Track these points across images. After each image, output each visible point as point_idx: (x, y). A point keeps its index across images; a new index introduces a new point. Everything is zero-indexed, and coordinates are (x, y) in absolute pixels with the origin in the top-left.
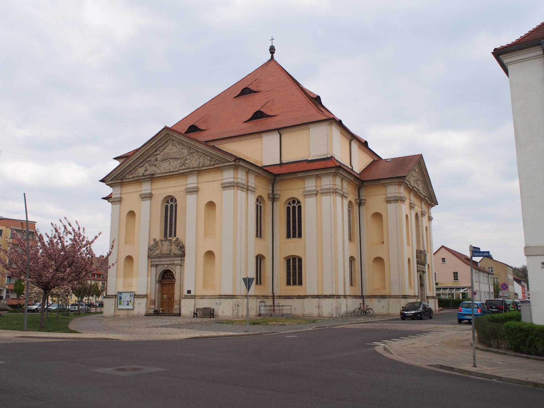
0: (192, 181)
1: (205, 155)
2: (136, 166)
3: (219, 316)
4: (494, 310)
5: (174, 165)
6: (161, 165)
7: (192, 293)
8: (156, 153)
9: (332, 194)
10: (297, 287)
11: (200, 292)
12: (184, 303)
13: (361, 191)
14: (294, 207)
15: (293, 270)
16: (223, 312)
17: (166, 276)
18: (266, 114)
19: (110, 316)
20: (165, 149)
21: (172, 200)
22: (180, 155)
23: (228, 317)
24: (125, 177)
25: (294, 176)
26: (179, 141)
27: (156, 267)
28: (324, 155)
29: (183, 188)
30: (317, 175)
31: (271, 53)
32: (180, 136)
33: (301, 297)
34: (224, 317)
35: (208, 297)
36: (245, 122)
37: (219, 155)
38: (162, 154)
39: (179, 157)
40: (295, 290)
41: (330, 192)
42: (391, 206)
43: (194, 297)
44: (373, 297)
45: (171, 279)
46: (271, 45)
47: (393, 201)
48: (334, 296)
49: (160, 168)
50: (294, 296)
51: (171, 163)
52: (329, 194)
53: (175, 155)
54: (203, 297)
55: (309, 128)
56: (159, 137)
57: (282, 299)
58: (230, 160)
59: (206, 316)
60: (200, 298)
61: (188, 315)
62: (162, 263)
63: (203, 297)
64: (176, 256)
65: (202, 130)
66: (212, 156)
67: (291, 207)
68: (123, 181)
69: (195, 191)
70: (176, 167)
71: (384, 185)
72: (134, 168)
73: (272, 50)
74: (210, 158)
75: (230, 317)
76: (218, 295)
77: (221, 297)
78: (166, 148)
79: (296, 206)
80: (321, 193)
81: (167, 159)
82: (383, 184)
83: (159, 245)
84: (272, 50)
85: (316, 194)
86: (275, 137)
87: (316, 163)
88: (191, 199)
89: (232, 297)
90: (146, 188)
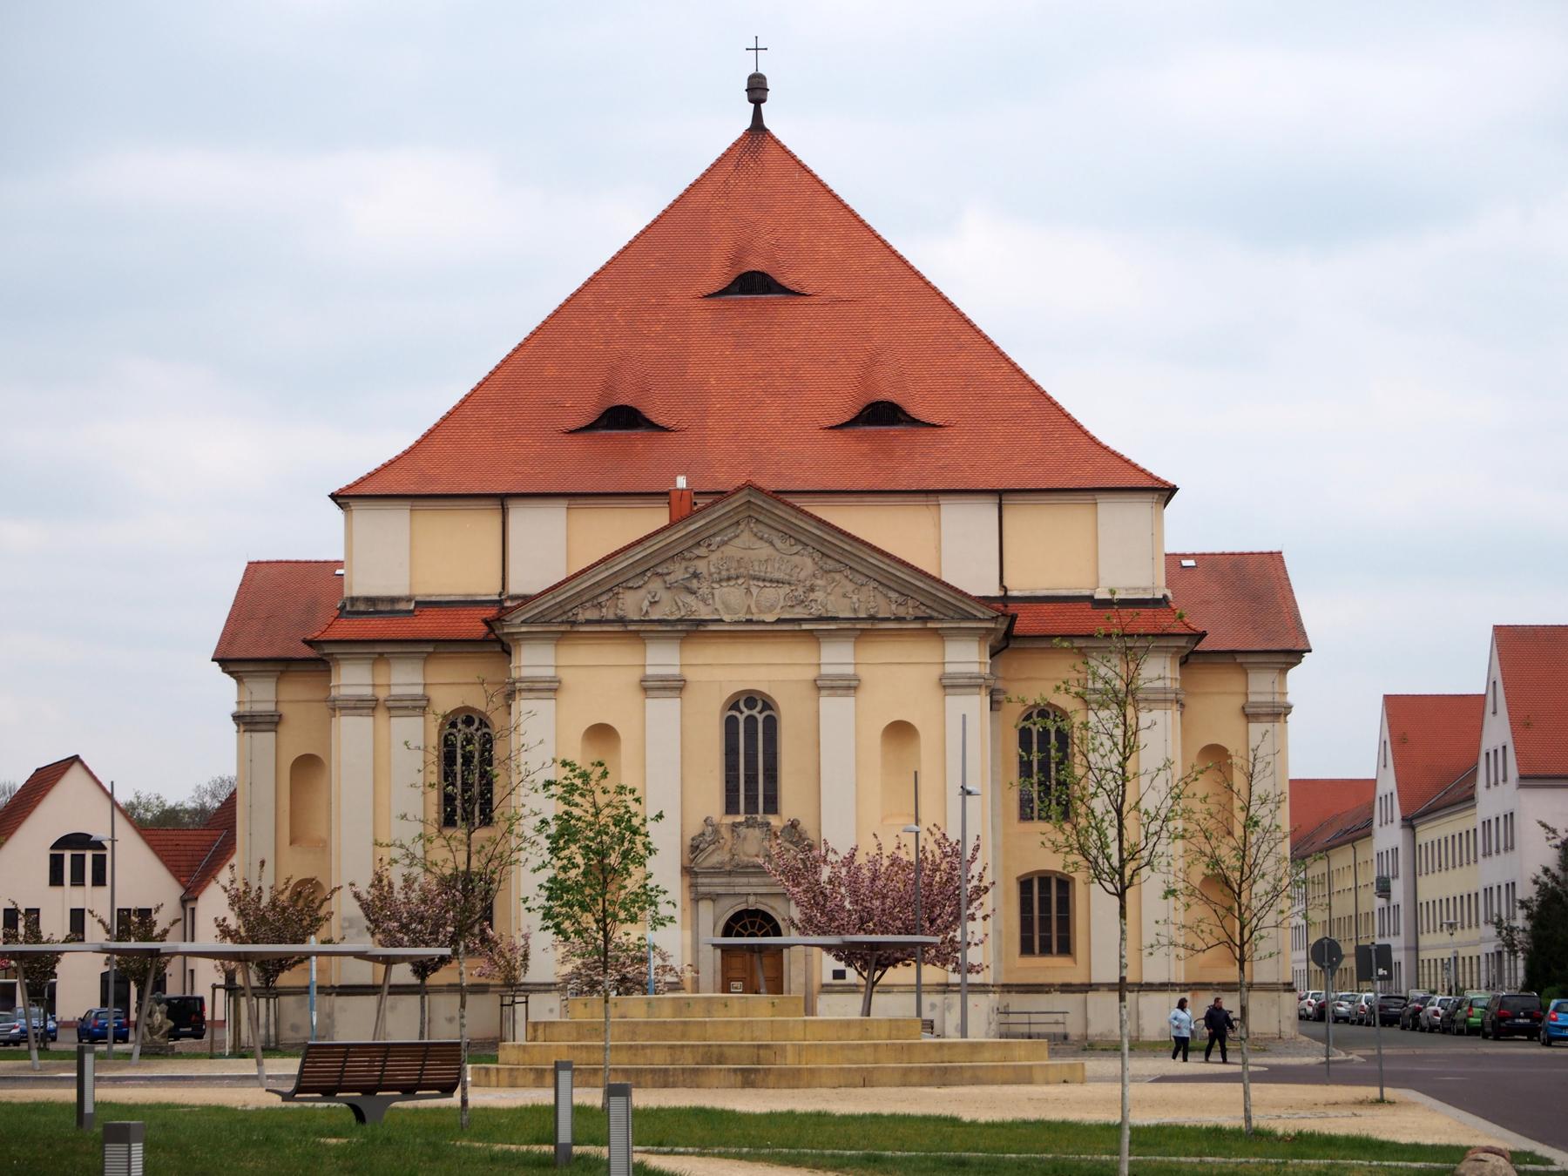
0: (837, 657)
1: (880, 583)
4: (1521, 1021)
5: (771, 603)
6: (716, 592)
8: (697, 552)
9: (1169, 705)
14: (751, 720)
15: (1041, 911)
17: (747, 921)
18: (909, 416)
20: (725, 543)
21: (469, 721)
22: (788, 571)
24: (570, 614)
25: (1044, 644)
26: (785, 530)
27: (714, 901)
28: (1145, 589)
29: (811, 674)
30: (381, 654)
31: (751, 101)
32: (801, 520)
33: (1073, 989)
35: (902, 989)
37: (941, 595)
38: (714, 557)
39: (787, 577)
40: (1053, 967)
41: (1165, 701)
42: (1256, 729)
44: (1198, 987)
46: (754, 71)
47: (1268, 715)
48: (1173, 984)
49: (711, 602)
50: (1052, 985)
51: (755, 591)
52: (1162, 705)
53: (769, 569)
56: (718, 510)
57: (1013, 994)
58: (980, 615)
62: (738, 890)
65: (662, 427)
66: (906, 592)
67: (741, 718)
68: (575, 629)
69: (848, 686)
70: (771, 609)
71: (1244, 669)
72: (611, 590)
73: (757, 89)
76: (934, 982)
78: (731, 543)
81: (737, 578)
82: (1241, 664)
84: (757, 89)
85: (374, 709)
86: (982, 514)
88: (834, 708)
89: (546, 988)
90: (663, 659)
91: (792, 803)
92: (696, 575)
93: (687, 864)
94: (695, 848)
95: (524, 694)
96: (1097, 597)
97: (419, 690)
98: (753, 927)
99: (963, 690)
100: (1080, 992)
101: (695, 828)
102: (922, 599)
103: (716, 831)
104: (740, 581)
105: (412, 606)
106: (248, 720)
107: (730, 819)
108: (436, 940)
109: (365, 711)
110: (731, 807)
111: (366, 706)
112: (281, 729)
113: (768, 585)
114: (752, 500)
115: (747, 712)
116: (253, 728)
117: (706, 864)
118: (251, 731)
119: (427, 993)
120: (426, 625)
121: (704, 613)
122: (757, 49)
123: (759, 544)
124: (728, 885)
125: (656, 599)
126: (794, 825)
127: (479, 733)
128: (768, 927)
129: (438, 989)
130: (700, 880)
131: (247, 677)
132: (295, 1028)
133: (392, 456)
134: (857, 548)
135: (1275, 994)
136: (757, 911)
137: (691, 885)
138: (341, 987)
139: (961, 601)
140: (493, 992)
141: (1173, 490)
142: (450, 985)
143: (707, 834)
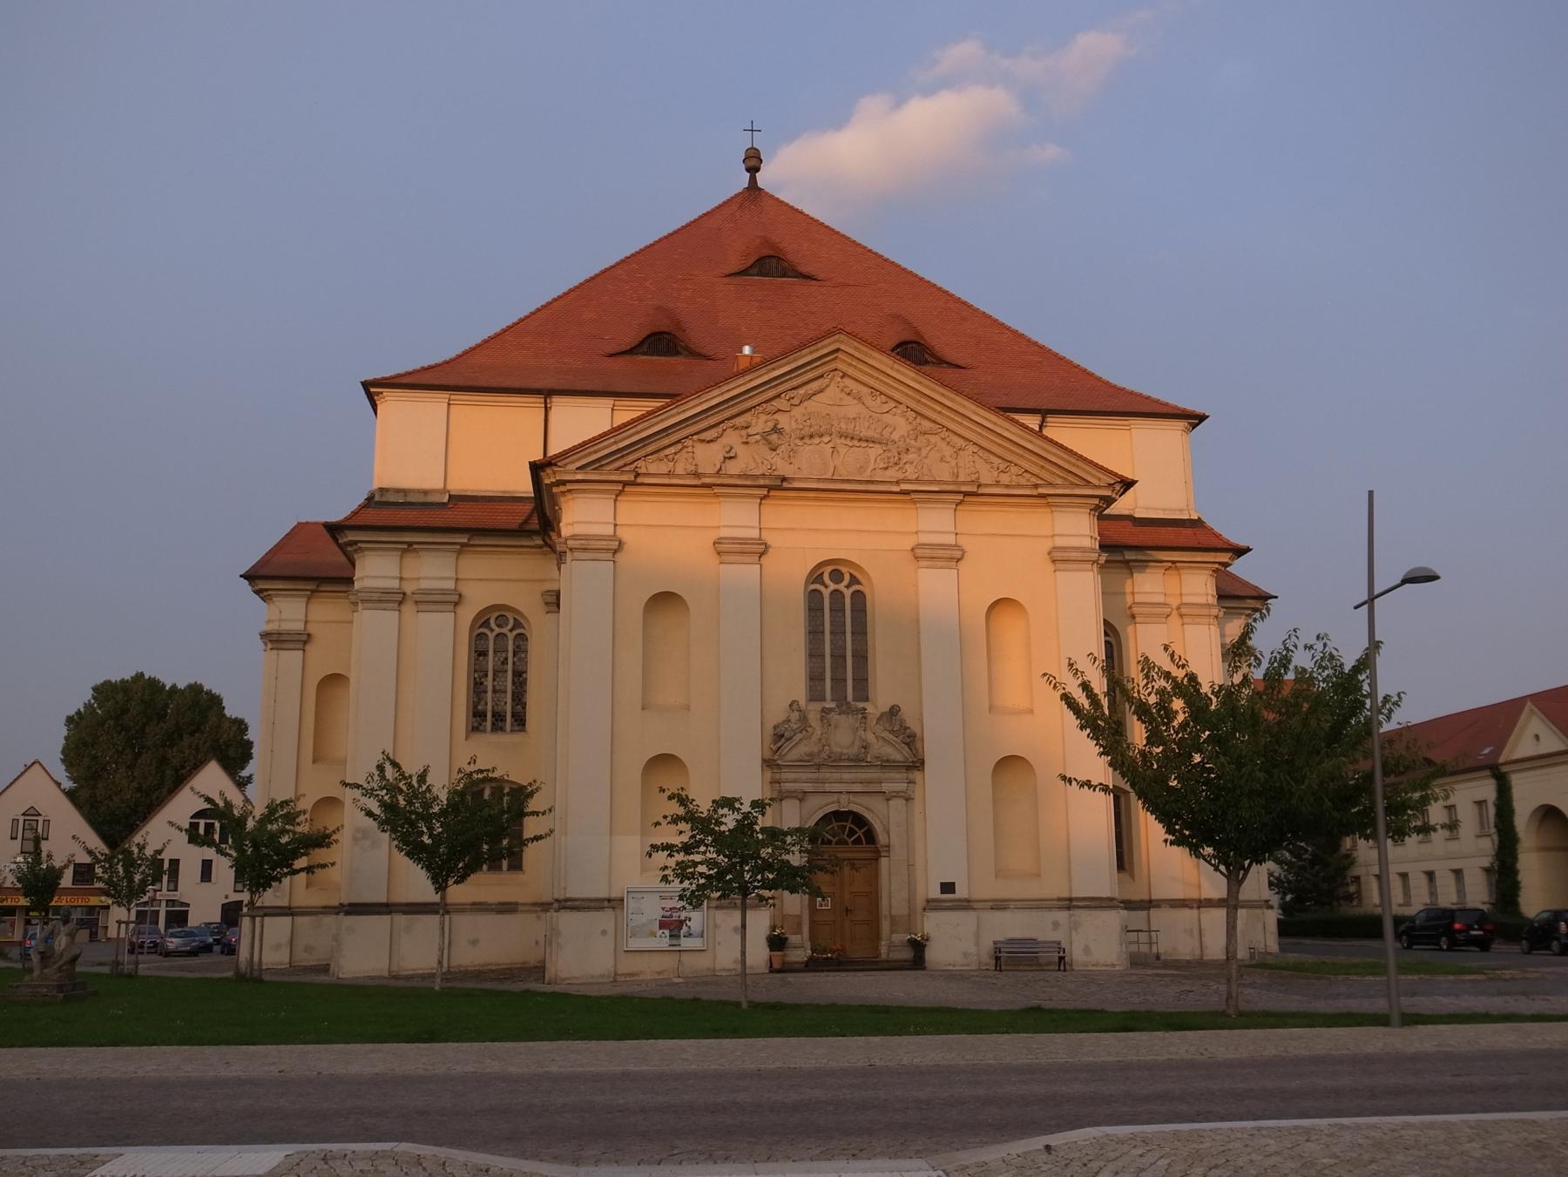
0: (936, 523)
2: (687, 437)
3: (1074, 963)
5: (850, 461)
7: (961, 892)
10: (505, 876)
11: (988, 889)
12: (937, 925)
13: (309, 607)
16: (1087, 951)
19: (593, 977)
23: (1107, 965)
27: (801, 800)
29: (910, 542)
30: (410, 544)
34: (1093, 965)
36: (611, 355)
38: (797, 412)
43: (966, 905)
45: (848, 844)
51: (843, 450)
54: (999, 905)
55: (1128, 428)
56: (805, 355)
59: (1020, 965)
60: (992, 909)
61: (954, 966)
62: (828, 787)
63: (999, 905)
64: (886, 765)
72: (679, 441)
74: (1000, 461)
75: (1113, 965)
76: (1055, 897)
77: (1069, 904)
79: (494, 633)
80: (416, 602)
81: (821, 436)
83: (810, 726)
84: (753, 163)
85: (400, 603)
87: (1163, 530)
89: (597, 904)
91: (883, 695)
92: (776, 430)
93: (768, 755)
94: (779, 737)
95: (577, 555)
96: (1136, 516)
97: (450, 585)
98: (850, 836)
99: (1075, 566)
100: (394, 905)
101: (778, 713)
102: (1026, 465)
103: (804, 718)
104: (826, 439)
105: (446, 499)
106: (275, 637)
107: (817, 706)
108: (497, 720)
109: (391, 605)
110: (815, 695)
111: (397, 599)
112: (308, 647)
113: (856, 443)
114: (842, 347)
115: (832, 586)
116: (280, 646)
117: (789, 757)
118: (278, 649)
119: (448, 912)
120: (460, 517)
121: (784, 469)
122: (752, 130)
123: (849, 400)
124: (816, 781)
125: (732, 455)
126: (894, 711)
127: (515, 633)
128: (860, 833)
129: (461, 909)
130: (784, 776)
131: (277, 596)
132: (308, 949)
133: (432, 363)
134: (960, 404)
135: (1258, 911)
136: (850, 812)
137: (773, 782)
138: (350, 905)
139: (1074, 465)
140: (523, 911)
141: (1202, 418)
142: (474, 904)
143: (793, 720)
